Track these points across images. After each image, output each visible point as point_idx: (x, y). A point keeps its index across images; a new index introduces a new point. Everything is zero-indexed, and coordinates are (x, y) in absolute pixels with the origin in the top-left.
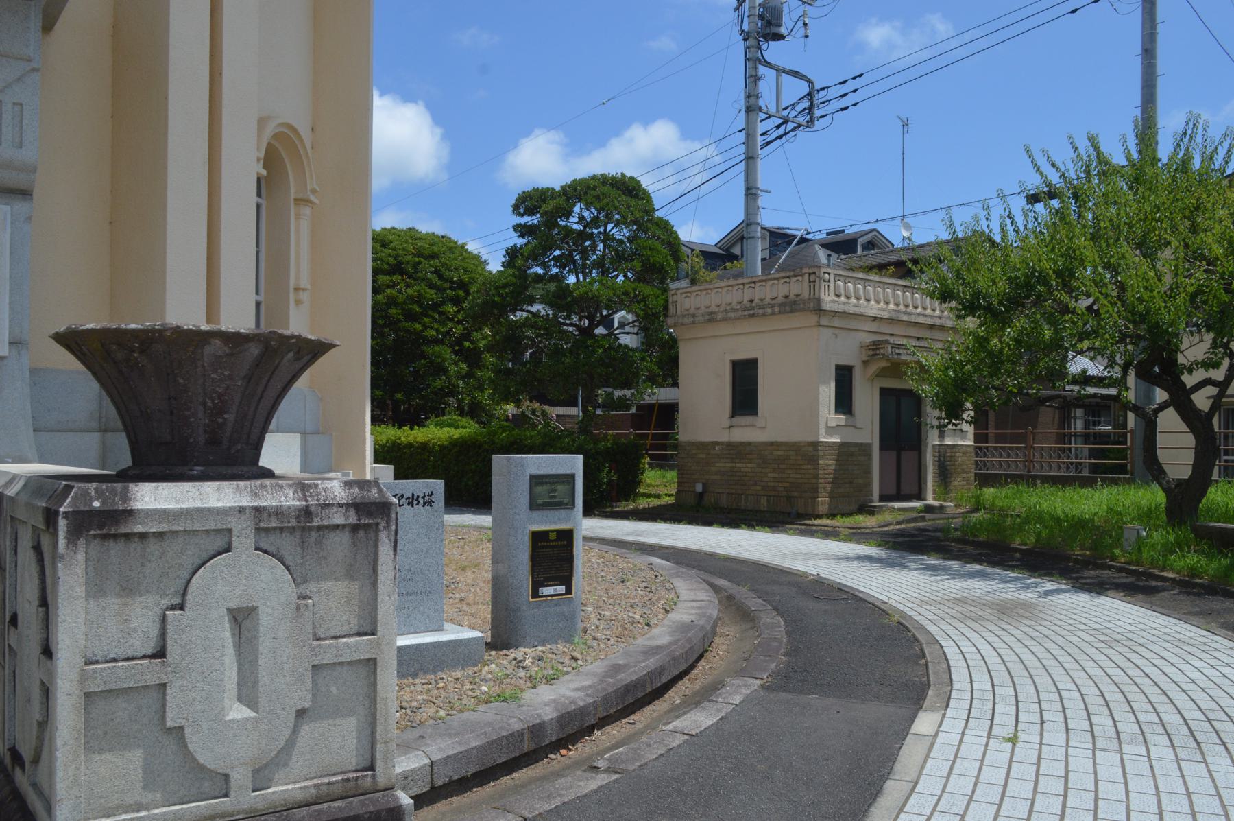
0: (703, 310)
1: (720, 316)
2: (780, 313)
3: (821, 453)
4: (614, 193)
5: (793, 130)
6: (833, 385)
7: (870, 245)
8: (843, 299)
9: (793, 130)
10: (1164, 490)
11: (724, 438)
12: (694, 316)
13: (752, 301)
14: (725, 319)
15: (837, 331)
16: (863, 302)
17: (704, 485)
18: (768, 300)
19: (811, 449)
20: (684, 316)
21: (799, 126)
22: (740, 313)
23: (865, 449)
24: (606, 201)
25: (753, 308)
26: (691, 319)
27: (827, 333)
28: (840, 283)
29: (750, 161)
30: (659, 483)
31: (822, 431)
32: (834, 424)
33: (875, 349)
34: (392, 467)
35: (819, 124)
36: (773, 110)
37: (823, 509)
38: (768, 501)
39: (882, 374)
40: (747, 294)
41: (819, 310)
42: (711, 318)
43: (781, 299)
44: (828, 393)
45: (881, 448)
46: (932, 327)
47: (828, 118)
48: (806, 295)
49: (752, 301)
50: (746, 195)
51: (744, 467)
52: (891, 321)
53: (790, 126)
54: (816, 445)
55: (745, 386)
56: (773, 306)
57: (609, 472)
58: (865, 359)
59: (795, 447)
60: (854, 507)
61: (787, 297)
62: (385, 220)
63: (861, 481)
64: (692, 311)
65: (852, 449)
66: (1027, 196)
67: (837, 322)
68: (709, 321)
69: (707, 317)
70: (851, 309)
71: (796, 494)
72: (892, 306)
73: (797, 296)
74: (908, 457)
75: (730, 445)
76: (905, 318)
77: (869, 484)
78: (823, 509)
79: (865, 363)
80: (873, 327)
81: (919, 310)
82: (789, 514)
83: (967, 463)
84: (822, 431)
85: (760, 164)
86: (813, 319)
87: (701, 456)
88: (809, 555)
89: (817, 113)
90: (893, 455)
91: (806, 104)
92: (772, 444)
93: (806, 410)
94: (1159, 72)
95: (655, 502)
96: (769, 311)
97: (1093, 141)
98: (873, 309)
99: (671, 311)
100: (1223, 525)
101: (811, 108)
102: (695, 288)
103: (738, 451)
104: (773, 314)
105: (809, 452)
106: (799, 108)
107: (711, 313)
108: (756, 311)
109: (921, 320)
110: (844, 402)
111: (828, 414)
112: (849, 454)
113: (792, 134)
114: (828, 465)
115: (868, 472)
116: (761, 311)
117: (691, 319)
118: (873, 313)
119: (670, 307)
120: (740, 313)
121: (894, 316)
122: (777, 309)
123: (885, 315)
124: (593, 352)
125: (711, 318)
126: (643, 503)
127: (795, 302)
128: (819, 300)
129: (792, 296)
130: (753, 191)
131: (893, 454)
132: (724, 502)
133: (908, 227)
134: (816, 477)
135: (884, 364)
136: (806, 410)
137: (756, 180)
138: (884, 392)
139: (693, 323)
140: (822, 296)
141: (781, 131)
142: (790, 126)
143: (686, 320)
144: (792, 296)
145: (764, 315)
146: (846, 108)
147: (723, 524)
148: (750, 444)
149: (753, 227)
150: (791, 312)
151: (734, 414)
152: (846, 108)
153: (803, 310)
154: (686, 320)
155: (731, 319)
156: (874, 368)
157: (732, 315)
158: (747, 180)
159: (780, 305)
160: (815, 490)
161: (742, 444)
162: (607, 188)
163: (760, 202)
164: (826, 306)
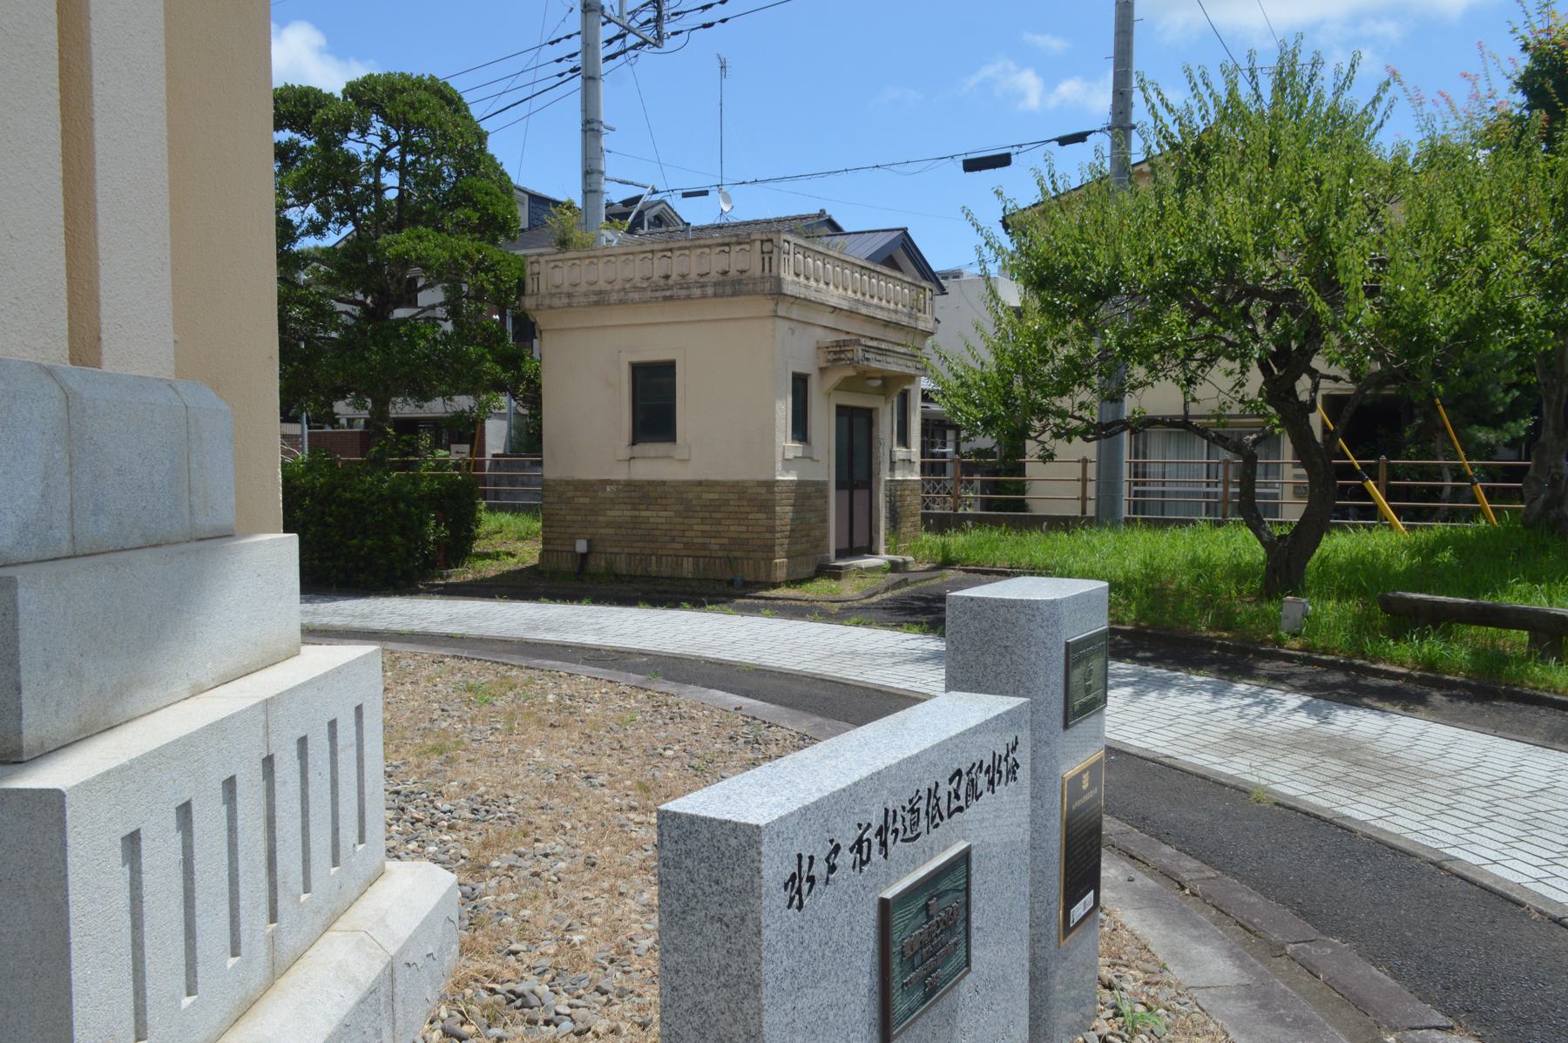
0: (583, 288)
1: (614, 297)
2: (715, 295)
3: (778, 497)
4: (435, 101)
5: (634, 48)
6: (790, 399)
7: (659, 221)
8: (802, 279)
9: (634, 48)
10: (1264, 544)
11: (621, 474)
12: (569, 295)
13: (667, 277)
14: (622, 302)
15: (793, 325)
16: (822, 285)
17: (589, 542)
18: (693, 276)
19: (763, 490)
20: (552, 295)
21: (645, 42)
22: (649, 294)
23: (820, 487)
24: (426, 112)
25: (670, 288)
26: (565, 301)
27: (783, 325)
28: (800, 257)
29: (590, 83)
30: (511, 539)
31: (779, 466)
32: (790, 455)
33: (838, 353)
34: (295, 536)
35: (668, 44)
36: (614, 14)
37: (781, 574)
38: (696, 565)
39: (846, 385)
40: (659, 267)
41: (777, 293)
42: (600, 300)
43: (714, 276)
44: (784, 410)
45: (838, 487)
46: (887, 324)
47: (682, 38)
48: (756, 270)
49: (667, 277)
50: (585, 131)
51: (654, 516)
52: (851, 313)
53: (632, 40)
54: (770, 485)
55: (653, 403)
56: (703, 286)
57: (437, 526)
58: (823, 365)
59: (739, 488)
60: (811, 569)
61: (725, 273)
62: (278, 82)
63: (817, 533)
64: (566, 288)
65: (809, 489)
66: (965, 162)
67: (795, 313)
68: (597, 303)
69: (595, 298)
70: (812, 296)
71: (738, 554)
72: (850, 292)
73: (742, 272)
74: (860, 495)
75: (630, 485)
76: (864, 311)
77: (825, 536)
78: (781, 574)
79: (822, 370)
80: (829, 320)
81: (875, 301)
82: (731, 583)
83: (913, 502)
84: (779, 466)
85: (605, 88)
86: (767, 306)
87: (582, 500)
88: (873, 658)
89: (668, 28)
90: (846, 493)
91: (650, 14)
92: (700, 483)
93: (747, 430)
94: (1136, 16)
95: (510, 564)
96: (697, 292)
97: (1316, 63)
98: (834, 296)
99: (529, 286)
100: (1442, 598)
101: (659, 19)
102: (568, 255)
103: (644, 493)
104: (704, 296)
105: (761, 495)
106: (643, 17)
107: (600, 292)
108: (676, 292)
109: (879, 314)
110: (800, 429)
111: (787, 446)
112: (806, 493)
113: (632, 53)
114: (785, 511)
115: (825, 520)
116: (683, 293)
117: (565, 301)
118: (833, 302)
119: (528, 281)
120: (649, 294)
121: (854, 308)
122: (710, 291)
123: (845, 305)
124: (413, 344)
125: (600, 300)
126: (490, 569)
127: (740, 282)
128: (779, 280)
129: (733, 273)
130: (595, 126)
131: (846, 493)
132: (622, 566)
133: (727, 199)
134: (772, 529)
135: (850, 372)
136: (747, 430)
137: (598, 112)
138: (841, 410)
139: (570, 305)
140: (783, 275)
141: (616, 47)
142: (632, 40)
143: (556, 302)
144: (733, 273)
145: (688, 297)
146: (711, 25)
147: (598, 599)
148: (663, 483)
149: (595, 176)
150: (734, 294)
151: (635, 441)
152: (711, 25)
153: (749, 293)
154: (556, 302)
155: (633, 302)
156: (835, 377)
157: (636, 296)
158: (585, 110)
159: (715, 284)
160: (770, 549)
161: (650, 483)
162: (424, 95)
163: (605, 142)
164: (789, 289)
